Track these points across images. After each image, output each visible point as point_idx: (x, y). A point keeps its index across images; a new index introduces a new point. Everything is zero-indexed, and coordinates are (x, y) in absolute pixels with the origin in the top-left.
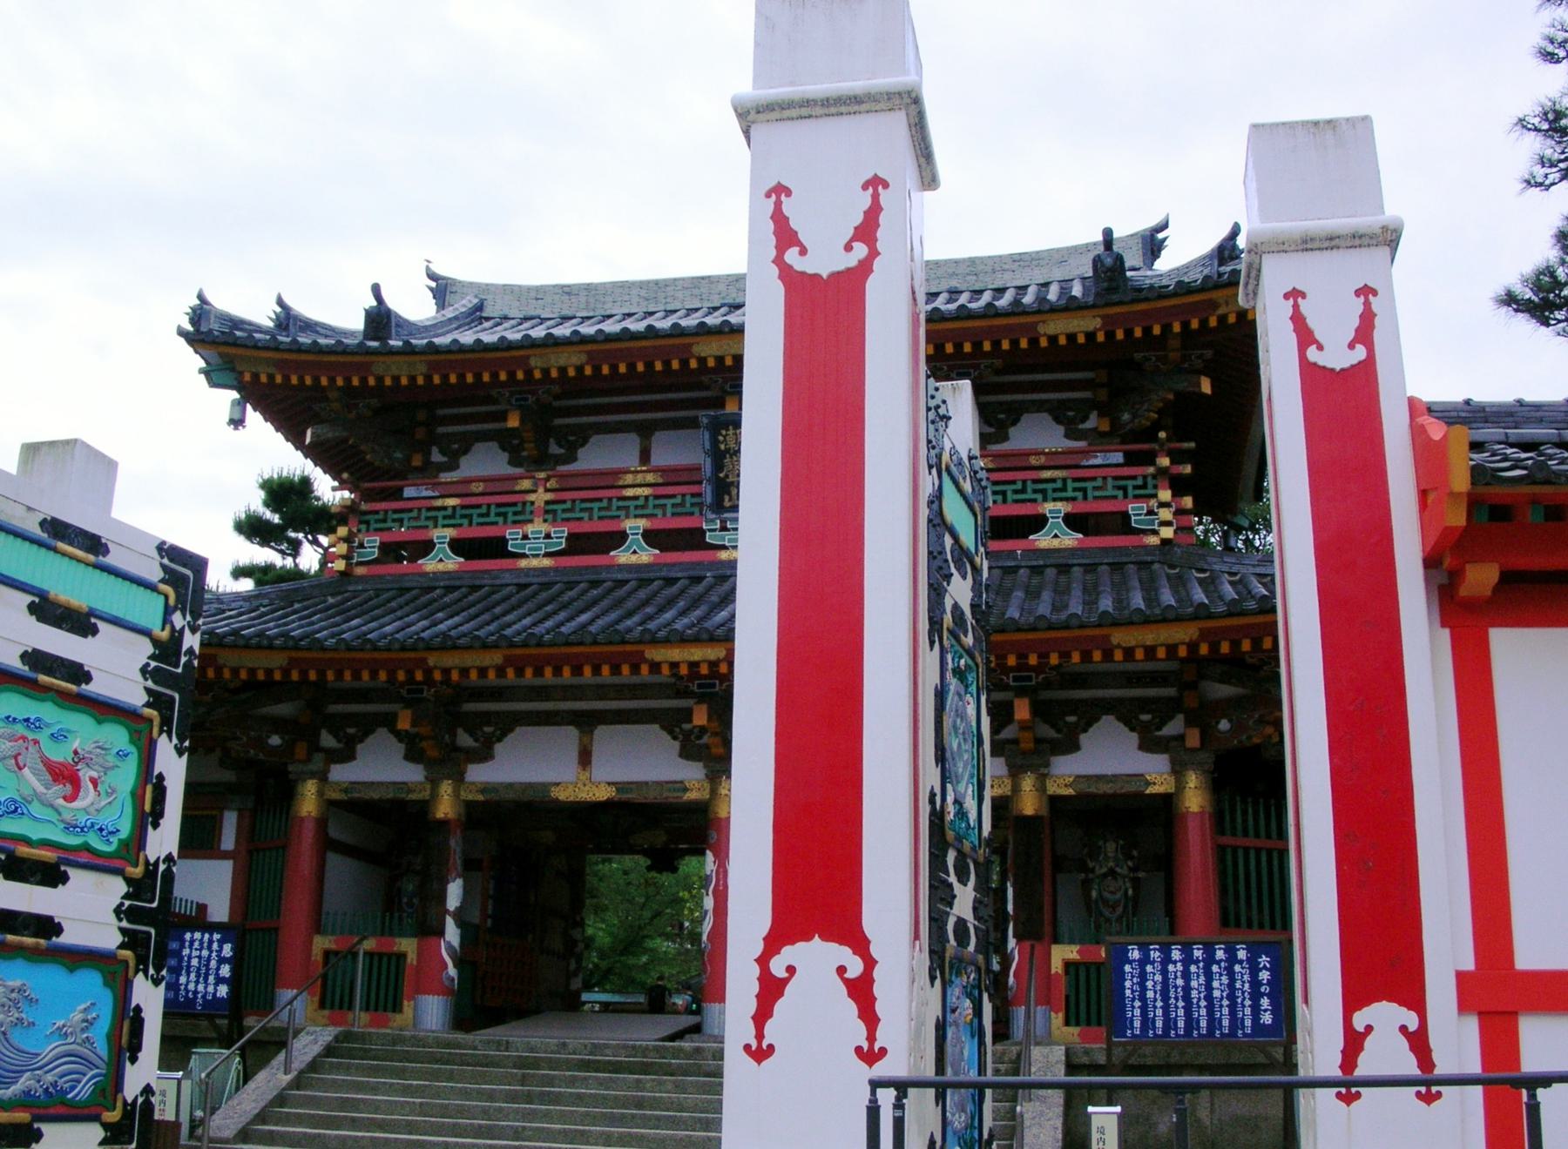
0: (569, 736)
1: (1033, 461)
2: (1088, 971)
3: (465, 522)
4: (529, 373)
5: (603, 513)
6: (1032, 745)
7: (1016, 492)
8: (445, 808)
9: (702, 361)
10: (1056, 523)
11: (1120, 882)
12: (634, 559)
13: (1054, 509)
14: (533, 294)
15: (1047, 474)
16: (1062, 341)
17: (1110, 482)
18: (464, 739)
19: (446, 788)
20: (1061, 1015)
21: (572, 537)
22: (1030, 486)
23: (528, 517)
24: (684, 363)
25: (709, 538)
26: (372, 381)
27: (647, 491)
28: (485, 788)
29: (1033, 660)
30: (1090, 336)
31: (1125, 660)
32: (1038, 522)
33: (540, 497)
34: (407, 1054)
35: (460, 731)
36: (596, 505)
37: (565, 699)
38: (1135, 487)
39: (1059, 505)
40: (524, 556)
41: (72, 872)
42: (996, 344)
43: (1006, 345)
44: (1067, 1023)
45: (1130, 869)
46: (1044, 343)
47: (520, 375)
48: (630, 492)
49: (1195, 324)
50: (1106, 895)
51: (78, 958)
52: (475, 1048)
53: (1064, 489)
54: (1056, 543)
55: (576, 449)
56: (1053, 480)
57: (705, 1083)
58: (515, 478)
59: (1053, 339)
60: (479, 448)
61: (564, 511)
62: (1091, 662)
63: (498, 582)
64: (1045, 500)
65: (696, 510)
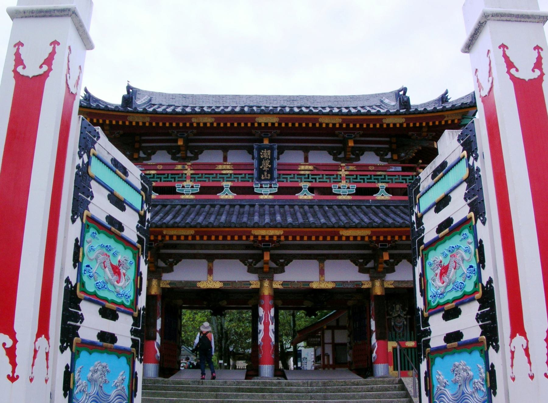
0: (315, 263)
1: (370, 168)
2: (411, 351)
3: (159, 180)
4: (191, 124)
5: (243, 179)
6: (268, 270)
7: (165, 178)
8: (266, 292)
9: (260, 124)
10: (382, 191)
11: (402, 320)
12: (226, 197)
13: (227, 184)
14: (171, 97)
15: (379, 173)
16: (391, 126)
17: (401, 177)
18: (161, 264)
19: (378, 283)
20: (392, 367)
21: (357, 189)
22: (373, 177)
23: (184, 179)
24: (124, 123)
25: (334, 191)
26: (127, 123)
27: (307, 172)
28: (284, 283)
29: (389, 238)
30: (273, 124)
31: (185, 240)
32: (376, 190)
33: (189, 172)
34: (180, 388)
35: (159, 260)
36: (211, 176)
37: (229, 249)
38: (368, 179)
39: (384, 184)
40: (261, 194)
41: (120, 315)
42: (361, 125)
43: (365, 126)
44: (394, 370)
45: (405, 315)
46: (385, 126)
47: (188, 125)
48: (302, 172)
49: (431, 124)
50: (397, 323)
51: (121, 351)
52: (189, 384)
53: (385, 179)
54: (383, 198)
55: (198, 155)
56: (381, 175)
57: (290, 395)
58: (175, 165)
59: (388, 125)
60: (159, 152)
61: (198, 178)
62: (172, 240)
63: (173, 203)
64: (378, 182)
65: (250, 180)
